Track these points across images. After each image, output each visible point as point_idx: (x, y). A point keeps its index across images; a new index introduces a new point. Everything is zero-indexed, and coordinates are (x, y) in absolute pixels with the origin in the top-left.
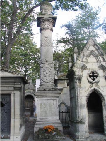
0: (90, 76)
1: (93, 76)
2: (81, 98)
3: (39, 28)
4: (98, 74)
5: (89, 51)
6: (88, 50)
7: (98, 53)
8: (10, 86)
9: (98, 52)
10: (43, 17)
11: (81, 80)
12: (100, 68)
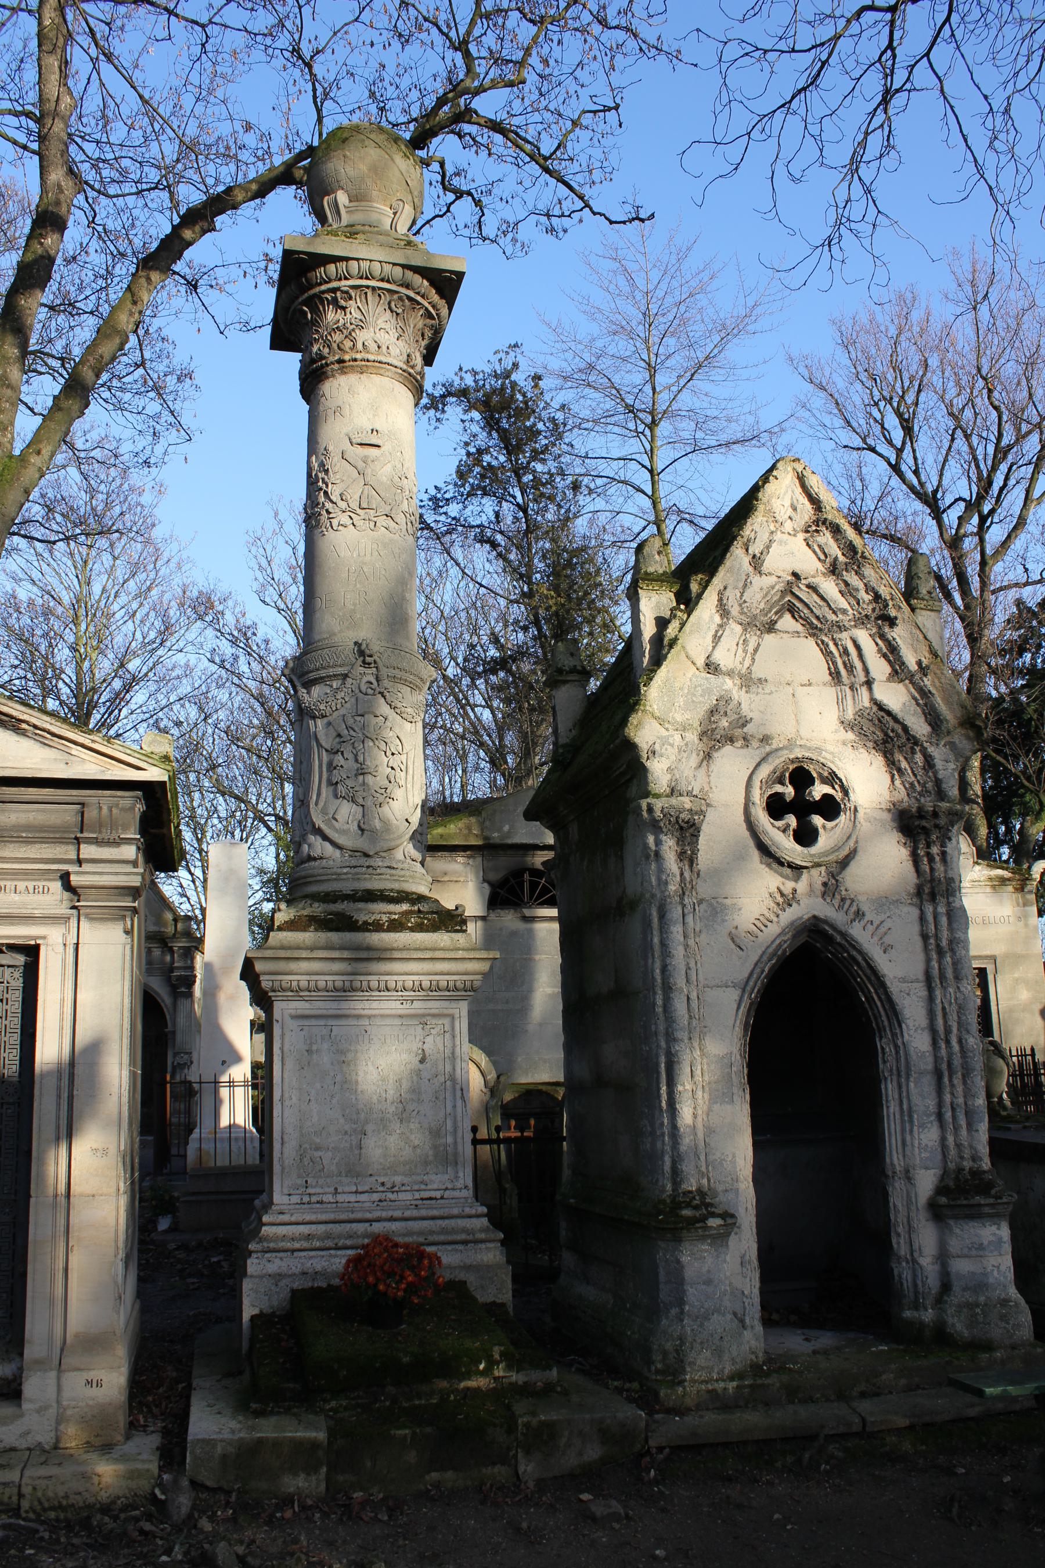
0: (776, 807)
1: (803, 808)
2: (694, 1004)
3: (292, 361)
4: (846, 792)
5: (767, 581)
6: (757, 562)
7: (843, 603)
8: (26, 874)
9: (848, 591)
10: (347, 259)
11: (696, 836)
12: (862, 734)
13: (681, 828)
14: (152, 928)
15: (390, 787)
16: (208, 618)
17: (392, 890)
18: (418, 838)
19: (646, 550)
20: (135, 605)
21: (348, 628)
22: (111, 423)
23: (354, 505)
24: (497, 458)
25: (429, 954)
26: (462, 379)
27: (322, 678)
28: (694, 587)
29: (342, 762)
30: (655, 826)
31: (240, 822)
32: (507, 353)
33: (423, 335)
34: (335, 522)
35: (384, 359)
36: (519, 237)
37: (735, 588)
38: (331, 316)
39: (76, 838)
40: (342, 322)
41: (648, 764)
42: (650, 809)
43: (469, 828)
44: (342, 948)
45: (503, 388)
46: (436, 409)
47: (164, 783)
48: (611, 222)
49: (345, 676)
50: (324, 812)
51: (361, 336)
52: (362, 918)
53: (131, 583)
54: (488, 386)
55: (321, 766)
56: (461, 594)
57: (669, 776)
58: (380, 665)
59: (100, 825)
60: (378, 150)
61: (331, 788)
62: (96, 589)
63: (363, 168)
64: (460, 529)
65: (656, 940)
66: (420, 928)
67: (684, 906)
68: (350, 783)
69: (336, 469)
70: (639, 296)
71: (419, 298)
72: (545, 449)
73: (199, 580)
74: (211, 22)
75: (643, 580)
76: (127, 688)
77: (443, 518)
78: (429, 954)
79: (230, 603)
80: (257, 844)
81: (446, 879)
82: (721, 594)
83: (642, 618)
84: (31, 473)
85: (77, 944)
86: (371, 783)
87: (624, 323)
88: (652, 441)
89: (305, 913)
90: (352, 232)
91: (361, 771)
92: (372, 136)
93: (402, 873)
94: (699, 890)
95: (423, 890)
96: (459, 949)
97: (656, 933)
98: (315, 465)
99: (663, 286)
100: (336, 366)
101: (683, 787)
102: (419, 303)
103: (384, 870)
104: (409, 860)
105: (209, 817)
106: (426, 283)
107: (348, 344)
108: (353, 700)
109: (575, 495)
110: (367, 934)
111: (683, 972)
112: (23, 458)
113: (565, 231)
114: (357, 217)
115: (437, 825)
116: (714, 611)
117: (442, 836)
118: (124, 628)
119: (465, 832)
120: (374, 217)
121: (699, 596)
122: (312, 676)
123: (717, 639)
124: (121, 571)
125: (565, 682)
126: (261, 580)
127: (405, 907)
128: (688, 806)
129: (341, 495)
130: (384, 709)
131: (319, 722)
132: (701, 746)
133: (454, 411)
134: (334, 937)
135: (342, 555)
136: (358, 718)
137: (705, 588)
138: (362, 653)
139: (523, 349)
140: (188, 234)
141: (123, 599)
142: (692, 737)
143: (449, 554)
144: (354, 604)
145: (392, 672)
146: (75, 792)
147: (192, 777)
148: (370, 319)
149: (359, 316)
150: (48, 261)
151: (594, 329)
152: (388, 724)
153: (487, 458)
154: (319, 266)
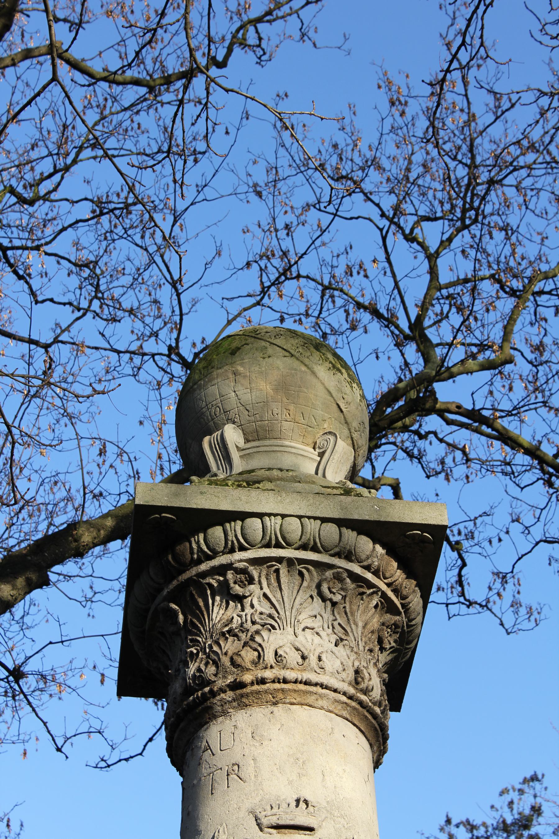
10: (243, 516)
32: (521, 792)
33: (380, 641)
35: (314, 678)
40: (237, 621)
60: (289, 360)
71: (369, 576)
74: (56, 341)
92: (278, 341)
100: (229, 695)
102: (370, 585)
106: (379, 549)
107: (249, 655)
120: (287, 461)
148: (286, 613)
149: (266, 608)
154: (196, 533)
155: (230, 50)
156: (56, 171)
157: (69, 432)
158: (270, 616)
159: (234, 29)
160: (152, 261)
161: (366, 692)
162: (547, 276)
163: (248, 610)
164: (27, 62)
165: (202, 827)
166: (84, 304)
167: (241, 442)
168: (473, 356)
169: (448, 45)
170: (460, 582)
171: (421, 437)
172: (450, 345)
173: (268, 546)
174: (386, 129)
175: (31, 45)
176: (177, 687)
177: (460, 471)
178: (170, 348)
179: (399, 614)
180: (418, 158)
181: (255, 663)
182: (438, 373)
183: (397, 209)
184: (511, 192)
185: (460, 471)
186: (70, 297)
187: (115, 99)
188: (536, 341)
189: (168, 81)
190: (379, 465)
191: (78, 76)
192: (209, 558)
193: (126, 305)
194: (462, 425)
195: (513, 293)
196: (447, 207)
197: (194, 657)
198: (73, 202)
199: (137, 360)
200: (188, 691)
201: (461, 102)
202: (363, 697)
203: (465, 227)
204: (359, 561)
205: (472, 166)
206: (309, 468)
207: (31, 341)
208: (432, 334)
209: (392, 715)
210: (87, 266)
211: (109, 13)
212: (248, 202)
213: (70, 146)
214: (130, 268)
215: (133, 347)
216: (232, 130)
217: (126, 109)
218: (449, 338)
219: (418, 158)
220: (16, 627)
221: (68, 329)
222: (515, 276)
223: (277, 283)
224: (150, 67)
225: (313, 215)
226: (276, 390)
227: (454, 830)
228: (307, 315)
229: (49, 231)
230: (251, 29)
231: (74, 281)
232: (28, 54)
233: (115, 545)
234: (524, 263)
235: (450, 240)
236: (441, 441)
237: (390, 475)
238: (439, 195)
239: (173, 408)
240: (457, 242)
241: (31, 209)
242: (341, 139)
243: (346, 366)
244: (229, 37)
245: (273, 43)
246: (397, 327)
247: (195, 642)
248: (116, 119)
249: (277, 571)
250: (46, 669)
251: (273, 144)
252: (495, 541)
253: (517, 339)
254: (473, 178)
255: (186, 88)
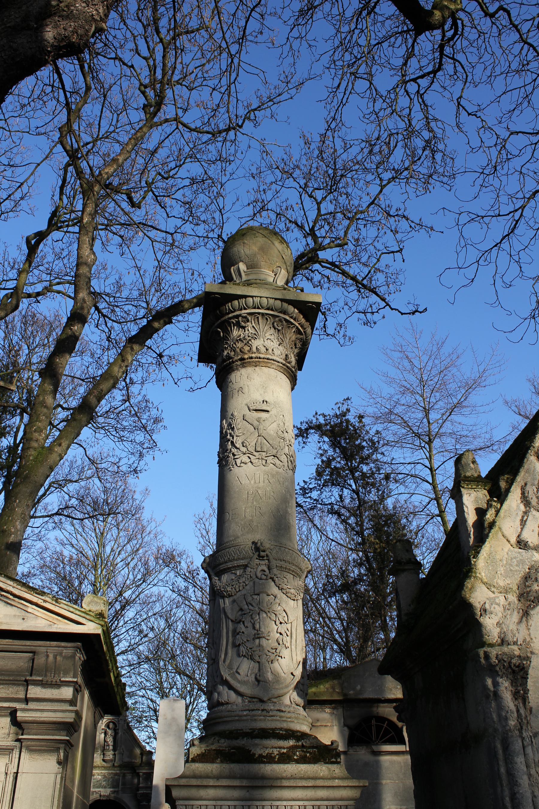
10: (246, 297)
11: (525, 678)
13: (514, 672)
14: (126, 760)
15: (279, 648)
16: (172, 565)
17: (281, 729)
18: (300, 688)
19: (464, 461)
20: (129, 559)
21: (248, 533)
22: (116, 448)
23: (252, 449)
24: (339, 463)
25: (310, 783)
26: (317, 419)
27: (229, 568)
28: (503, 484)
29: (243, 629)
30: (492, 671)
31: (189, 692)
32: (343, 404)
33: (295, 345)
34: (238, 461)
35: (270, 357)
36: (348, 334)
37: (533, 485)
38: (236, 333)
39: (26, 681)
40: (242, 336)
41: (481, 620)
42: (487, 656)
43: (333, 688)
44: (242, 777)
45: (342, 422)
46: (303, 437)
47: (99, 635)
48: (402, 314)
49: (245, 566)
50: (230, 667)
51: (255, 343)
52: (258, 751)
53: (128, 546)
54: (332, 423)
55: (227, 633)
56: (320, 549)
57: (498, 630)
58: (271, 558)
59: (46, 670)
60: (264, 239)
61: (235, 649)
62: (108, 549)
63: (255, 249)
64: (319, 506)
65: (503, 770)
66: (303, 760)
67: (523, 739)
68: (249, 645)
69: (239, 427)
70: (416, 370)
71: (292, 320)
72: (369, 457)
73: (167, 543)
74: (176, 232)
75: (464, 481)
76: (123, 608)
77: (308, 500)
78: (310, 783)
79: (184, 557)
80: (200, 706)
81: (318, 724)
82: (523, 489)
83: (465, 509)
84: (54, 457)
85: (17, 773)
86: (265, 645)
87: (409, 386)
88: (430, 452)
89: (213, 747)
90: (248, 283)
91: (258, 636)
92: (260, 231)
93: (289, 715)
94: (533, 724)
95: (305, 728)
96: (334, 778)
97: (501, 763)
98: (225, 425)
99: (430, 364)
100: (239, 363)
101: (509, 638)
102: (292, 324)
103: (275, 713)
104: (294, 705)
105: (171, 688)
106: (296, 311)
107: (247, 348)
108: (251, 583)
109: (387, 483)
110: (262, 765)
111: (530, 800)
112: (50, 449)
113: (375, 323)
114: (251, 277)
115: (311, 686)
116: (519, 501)
117: (315, 693)
118: (122, 572)
119: (331, 690)
120: (262, 277)
121: (508, 491)
122: (222, 567)
123: (523, 523)
124: (122, 540)
125: (404, 570)
126: (203, 543)
127: (291, 743)
128: (517, 653)
129: (243, 443)
130: (275, 590)
131: (227, 600)
132: (520, 605)
133: (314, 437)
134: (236, 767)
135: (243, 483)
136: (255, 597)
137: (511, 484)
138: (257, 549)
139: (352, 400)
140: (156, 325)
141: (123, 555)
142: (513, 598)
143: (312, 522)
144: (252, 516)
145: (279, 563)
146: (28, 643)
147: (162, 663)
148: (261, 333)
149: (253, 331)
150: (75, 338)
151: (392, 391)
152: (277, 601)
153: (333, 464)
155: (244, 121)
156: (176, 167)
157: (180, 267)
158: (255, 334)
159: (245, 113)
160: (212, 202)
161: (289, 363)
162: (362, 212)
163: (247, 332)
164: (166, 124)
165: (228, 410)
166: (186, 218)
167: (245, 269)
168: (333, 242)
169: (327, 122)
170: (325, 327)
171: (312, 272)
172: (324, 237)
173: (255, 308)
174: (303, 153)
175: (168, 117)
176: (220, 360)
177: (326, 285)
178: (219, 235)
179: (302, 334)
180: (314, 165)
181: (249, 351)
182: (320, 248)
183: (306, 184)
184: (349, 180)
185: (326, 285)
186: (181, 215)
187: (200, 139)
188: (356, 237)
189: (220, 132)
190: (296, 282)
191: (185, 129)
192: (233, 312)
193: (202, 219)
194: (327, 268)
195: (349, 218)
196: (325, 185)
197: (226, 348)
198: (183, 179)
199: (206, 240)
200: (224, 361)
201: (331, 145)
202: (288, 365)
203: (332, 193)
204: (288, 315)
205: (335, 170)
206: (271, 280)
207: (166, 232)
208: (318, 233)
209: (299, 372)
210: (188, 203)
211: (198, 106)
212: (147, 490)
213: (182, 157)
214: (204, 205)
215: (205, 235)
216: (244, 152)
217: (204, 143)
218: (324, 235)
219: (314, 165)
220: (160, 340)
221: (180, 228)
222: (350, 212)
223: (259, 212)
224: (213, 127)
225: (274, 186)
226: (259, 250)
227: (318, 417)
228: (271, 224)
229: (174, 190)
230: (252, 113)
231: (183, 209)
232: (166, 121)
233: (197, 309)
234: (353, 207)
235: (326, 197)
236: (320, 273)
237: (300, 286)
238: (322, 180)
239: (220, 258)
240: (328, 198)
241: (167, 181)
242: (285, 157)
243: (285, 242)
244: (244, 116)
245: (260, 119)
246: (305, 230)
247: (227, 343)
248: (199, 147)
249: (258, 318)
250: (171, 354)
251: (259, 158)
252: (338, 312)
253: (349, 236)
254: (335, 173)
255: (227, 134)
